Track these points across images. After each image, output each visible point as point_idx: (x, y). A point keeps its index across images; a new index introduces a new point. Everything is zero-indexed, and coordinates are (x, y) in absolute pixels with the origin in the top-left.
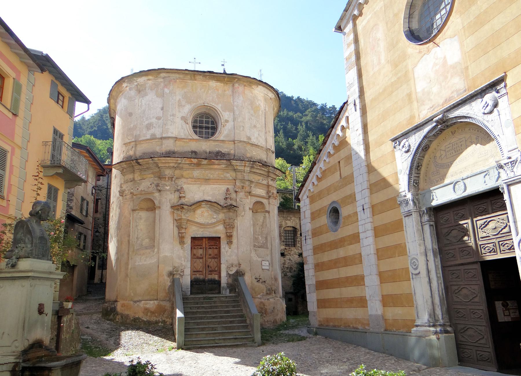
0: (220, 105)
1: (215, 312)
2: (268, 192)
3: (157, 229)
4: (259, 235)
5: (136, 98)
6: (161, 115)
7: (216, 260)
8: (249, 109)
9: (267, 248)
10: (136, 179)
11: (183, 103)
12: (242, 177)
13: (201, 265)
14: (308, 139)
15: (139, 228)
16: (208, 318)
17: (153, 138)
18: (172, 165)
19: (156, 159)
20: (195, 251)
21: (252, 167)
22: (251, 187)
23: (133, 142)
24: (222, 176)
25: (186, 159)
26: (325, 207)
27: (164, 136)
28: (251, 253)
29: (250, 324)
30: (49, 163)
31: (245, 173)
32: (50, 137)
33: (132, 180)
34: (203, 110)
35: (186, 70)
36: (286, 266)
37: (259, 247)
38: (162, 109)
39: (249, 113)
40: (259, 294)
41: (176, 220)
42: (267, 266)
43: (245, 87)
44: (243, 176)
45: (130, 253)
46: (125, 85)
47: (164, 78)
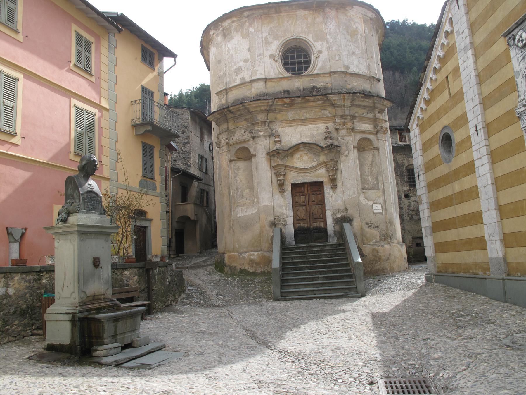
0: (311, 35)
3: (254, 178)
4: (368, 176)
6: (249, 57)
8: (344, 34)
9: (378, 189)
10: (230, 128)
11: (270, 40)
15: (238, 178)
17: (243, 84)
18: (263, 108)
20: (297, 199)
22: (354, 122)
25: (277, 100)
26: (437, 134)
27: (253, 78)
29: (354, 273)
30: (139, 122)
32: (138, 95)
33: (226, 129)
34: (293, 44)
36: (412, 208)
37: (370, 189)
38: (249, 50)
42: (379, 209)
43: (338, 11)
46: (211, 33)
47: (248, 17)
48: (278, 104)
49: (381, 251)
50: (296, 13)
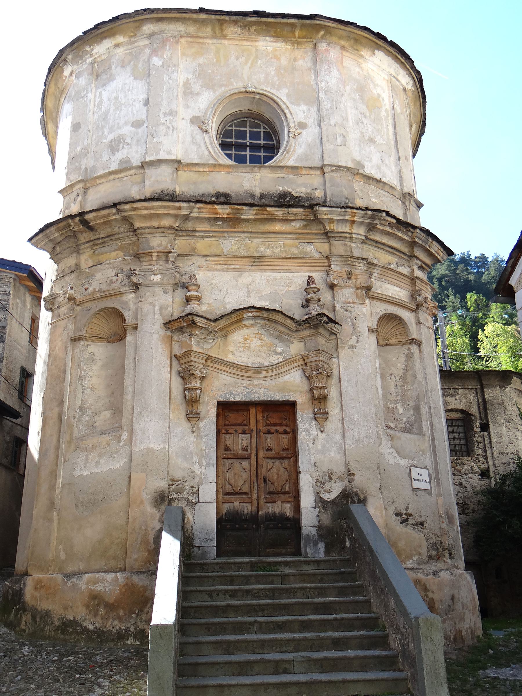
0: (285, 91)
1: (285, 609)
2: (413, 296)
3: (128, 381)
4: (396, 402)
5: (89, 89)
7: (286, 463)
8: (354, 100)
9: (421, 434)
10: (83, 266)
11: (196, 87)
12: (346, 251)
13: (244, 475)
14: (446, 302)
15: (87, 383)
16: (262, 628)
18: (166, 222)
19: (127, 207)
20: (228, 440)
21: (371, 227)
23: (79, 182)
24: (295, 251)
28: (380, 445)
31: (354, 241)
34: (245, 106)
35: (202, 10)
38: (146, 103)
39: (357, 109)
40: (410, 557)
41: (176, 356)
42: (425, 481)
43: (345, 53)
44: (348, 249)
45: (63, 446)
46: (67, 71)
47: (150, 36)
48: (202, 215)
49: (435, 588)
50: (257, 44)
